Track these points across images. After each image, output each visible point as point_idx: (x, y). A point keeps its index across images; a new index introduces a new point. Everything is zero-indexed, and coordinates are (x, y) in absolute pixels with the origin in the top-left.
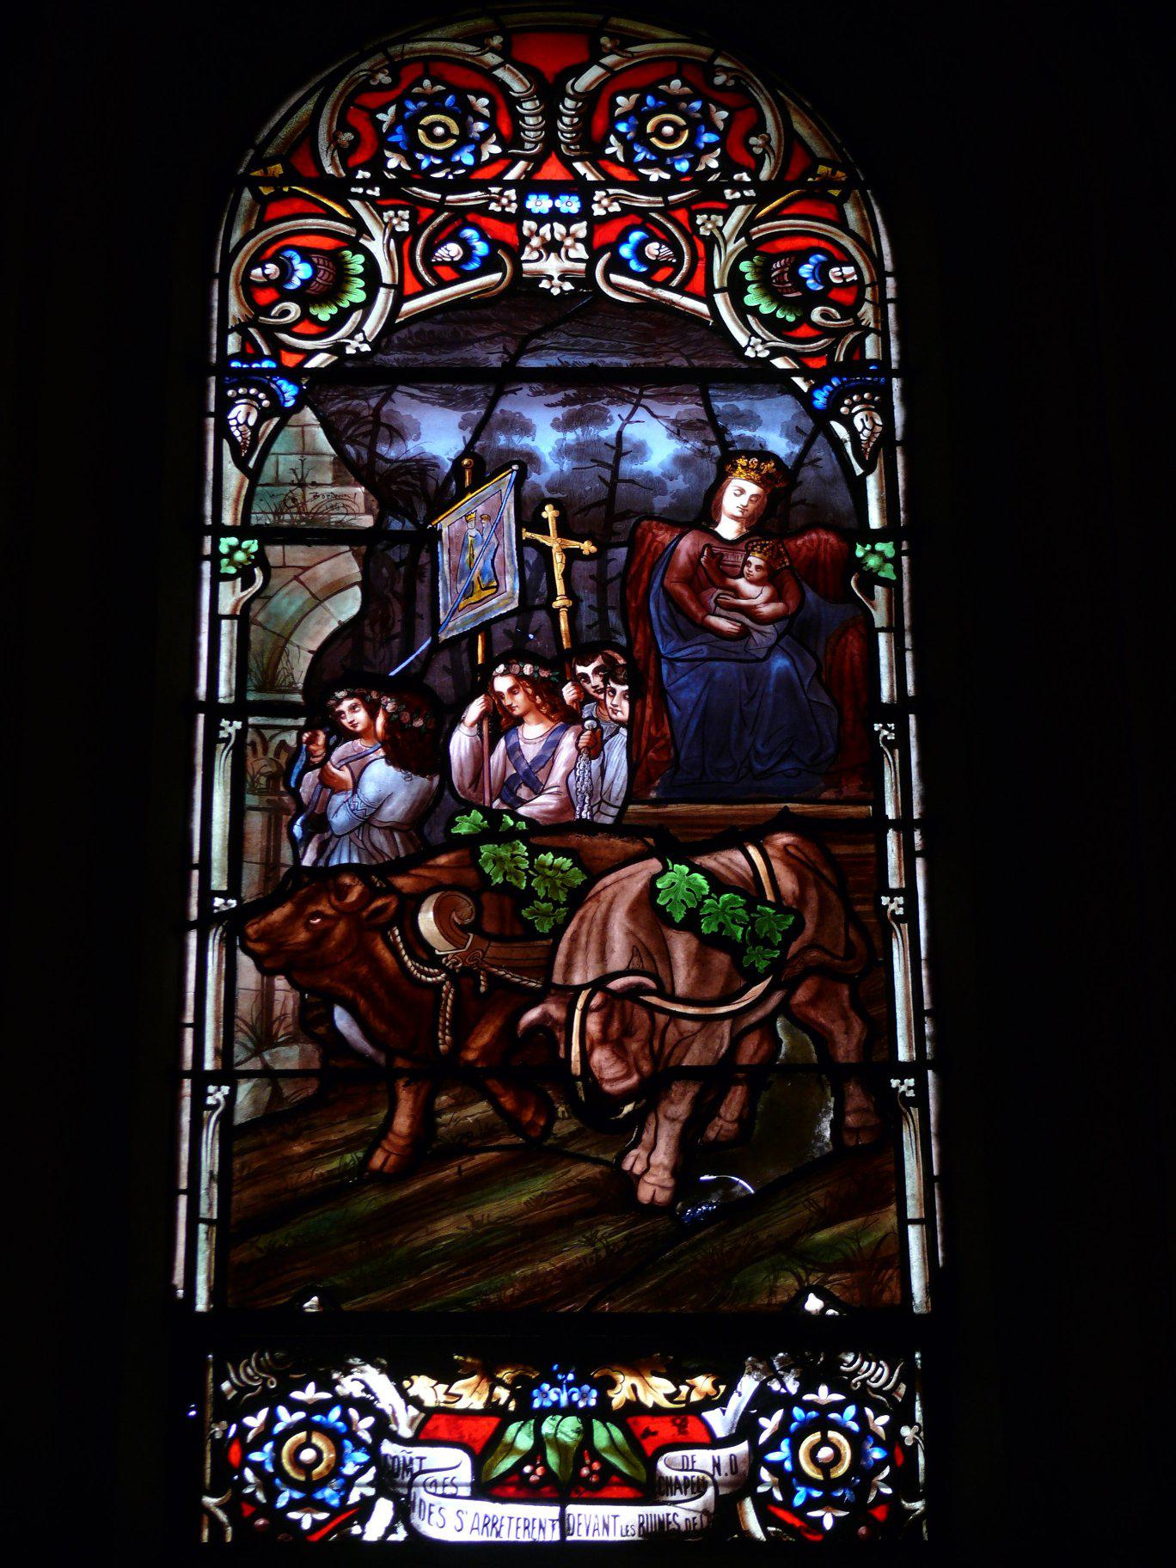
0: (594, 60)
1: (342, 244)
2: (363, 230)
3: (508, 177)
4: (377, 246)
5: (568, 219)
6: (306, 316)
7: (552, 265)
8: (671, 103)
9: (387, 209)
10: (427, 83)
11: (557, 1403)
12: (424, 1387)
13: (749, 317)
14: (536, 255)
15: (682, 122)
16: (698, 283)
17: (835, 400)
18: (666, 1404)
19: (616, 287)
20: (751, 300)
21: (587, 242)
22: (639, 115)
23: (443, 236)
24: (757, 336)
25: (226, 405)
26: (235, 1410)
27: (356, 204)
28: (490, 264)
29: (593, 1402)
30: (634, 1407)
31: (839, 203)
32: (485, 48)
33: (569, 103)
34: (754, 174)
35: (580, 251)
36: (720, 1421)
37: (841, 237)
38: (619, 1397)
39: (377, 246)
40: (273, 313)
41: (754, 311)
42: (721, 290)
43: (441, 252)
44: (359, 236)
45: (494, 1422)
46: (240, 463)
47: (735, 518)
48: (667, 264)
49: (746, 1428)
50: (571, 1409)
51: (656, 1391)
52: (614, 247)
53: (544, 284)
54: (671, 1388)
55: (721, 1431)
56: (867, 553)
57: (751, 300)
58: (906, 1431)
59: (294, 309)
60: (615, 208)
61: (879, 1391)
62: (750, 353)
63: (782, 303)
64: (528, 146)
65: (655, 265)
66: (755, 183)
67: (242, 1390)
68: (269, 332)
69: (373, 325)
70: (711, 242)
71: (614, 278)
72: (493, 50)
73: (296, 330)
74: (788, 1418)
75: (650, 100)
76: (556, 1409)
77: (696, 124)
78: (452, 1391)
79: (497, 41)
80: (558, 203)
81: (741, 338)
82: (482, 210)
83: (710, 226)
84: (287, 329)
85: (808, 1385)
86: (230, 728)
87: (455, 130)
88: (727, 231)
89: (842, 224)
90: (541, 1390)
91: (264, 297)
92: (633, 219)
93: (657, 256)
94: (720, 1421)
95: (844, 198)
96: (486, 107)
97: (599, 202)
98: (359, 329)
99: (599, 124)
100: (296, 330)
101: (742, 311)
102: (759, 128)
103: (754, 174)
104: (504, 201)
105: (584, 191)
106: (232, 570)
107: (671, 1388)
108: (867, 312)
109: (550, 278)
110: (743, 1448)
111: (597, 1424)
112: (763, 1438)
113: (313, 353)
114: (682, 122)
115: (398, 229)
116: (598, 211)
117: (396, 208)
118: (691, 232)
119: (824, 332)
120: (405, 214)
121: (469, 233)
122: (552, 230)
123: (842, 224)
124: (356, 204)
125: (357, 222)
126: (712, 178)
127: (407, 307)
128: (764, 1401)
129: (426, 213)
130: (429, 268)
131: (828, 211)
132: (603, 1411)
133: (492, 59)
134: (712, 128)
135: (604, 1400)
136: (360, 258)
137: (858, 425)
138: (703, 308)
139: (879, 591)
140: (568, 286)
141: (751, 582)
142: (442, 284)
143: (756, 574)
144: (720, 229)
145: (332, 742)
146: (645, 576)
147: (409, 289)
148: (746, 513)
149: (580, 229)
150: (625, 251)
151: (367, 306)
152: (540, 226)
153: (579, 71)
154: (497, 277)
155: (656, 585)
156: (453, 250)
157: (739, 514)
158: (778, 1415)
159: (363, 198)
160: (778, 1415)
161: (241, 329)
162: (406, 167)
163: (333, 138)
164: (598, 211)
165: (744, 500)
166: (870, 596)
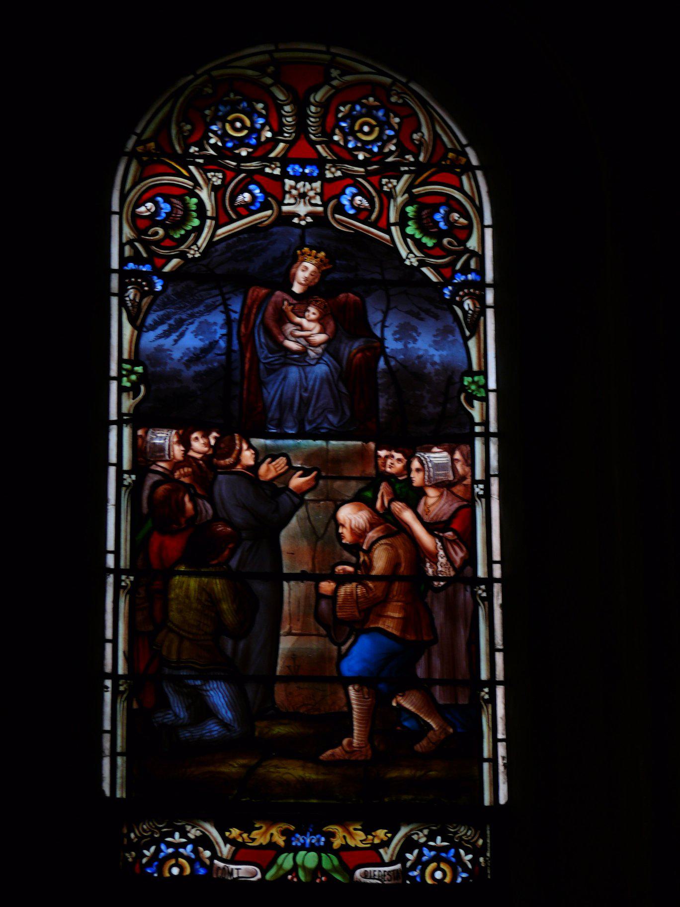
0: (328, 80)
1: (186, 192)
2: (197, 184)
3: (272, 155)
4: (204, 194)
5: (310, 179)
6: (167, 236)
7: (302, 209)
8: (369, 111)
9: (210, 171)
10: (232, 95)
11: (304, 844)
12: (235, 832)
13: (409, 240)
14: (292, 201)
15: (374, 122)
16: (383, 223)
17: (454, 294)
18: (361, 845)
19: (339, 222)
20: (410, 230)
21: (321, 195)
22: (351, 118)
23: (238, 190)
24: (412, 253)
25: (121, 295)
26: (139, 848)
27: (192, 168)
28: (265, 206)
29: (322, 844)
30: (345, 847)
31: (459, 176)
32: (265, 74)
33: (313, 109)
34: (416, 156)
35: (318, 200)
36: (387, 854)
37: (454, 193)
38: (337, 843)
39: (204, 194)
40: (150, 233)
41: (412, 237)
42: (394, 224)
43: (240, 198)
44: (195, 187)
45: (272, 853)
46: (132, 321)
47: (301, 284)
48: (365, 209)
49: (400, 858)
50: (312, 848)
51: (358, 839)
52: (338, 196)
53: (296, 220)
54: (364, 837)
55: (387, 858)
56: (470, 383)
57: (410, 230)
58: (481, 859)
59: (161, 232)
60: (339, 174)
61: (467, 842)
62: (407, 263)
63: (425, 232)
64: (286, 135)
65: (359, 209)
66: (417, 163)
67: (140, 838)
68: (146, 244)
69: (203, 242)
70: (391, 195)
71: (337, 216)
72: (270, 76)
73: (162, 244)
74: (421, 854)
75: (358, 108)
76: (303, 847)
77: (384, 124)
78: (251, 837)
79: (271, 69)
80: (301, 170)
81: (403, 253)
82: (261, 171)
83: (390, 185)
84: (157, 243)
85: (431, 837)
86: (128, 479)
87: (248, 123)
88: (398, 189)
89: (461, 190)
90: (295, 837)
91: (141, 224)
92: (350, 181)
93: (359, 205)
94: (387, 854)
95: (461, 174)
96: (263, 109)
97: (329, 170)
98: (195, 243)
99: (330, 121)
100: (162, 244)
101: (405, 236)
102: (418, 129)
103: (416, 156)
104: (311, 193)
105: (320, 163)
106: (128, 385)
107: (364, 837)
108: (473, 244)
109: (298, 216)
110: (398, 866)
111: (323, 855)
112: (409, 864)
113: (169, 259)
114: (374, 122)
115: (216, 184)
116: (329, 175)
117: (215, 171)
118: (379, 188)
119: (448, 252)
120: (220, 175)
121: (252, 187)
122: (304, 185)
123: (461, 190)
124: (192, 168)
125: (192, 178)
126: (390, 159)
127: (220, 231)
128: (409, 844)
129: (230, 174)
130: (234, 208)
131: (453, 180)
132: (328, 848)
133: (268, 81)
134: (391, 127)
135: (329, 844)
136: (195, 200)
137: (466, 307)
138: (387, 237)
139: (476, 403)
140: (309, 220)
141: (309, 321)
142: (241, 217)
143: (313, 317)
144: (395, 187)
145: (150, 463)
146: (253, 317)
147: (222, 221)
148: (308, 282)
149: (317, 185)
150: (345, 201)
151: (199, 230)
152: (297, 182)
153: (316, 90)
154: (269, 212)
155: (258, 321)
156: (247, 197)
157: (303, 282)
158: (416, 852)
159: (198, 166)
160: (416, 852)
161: (130, 242)
162: (220, 144)
163: (180, 130)
164: (329, 175)
165: (307, 274)
166: (472, 406)
